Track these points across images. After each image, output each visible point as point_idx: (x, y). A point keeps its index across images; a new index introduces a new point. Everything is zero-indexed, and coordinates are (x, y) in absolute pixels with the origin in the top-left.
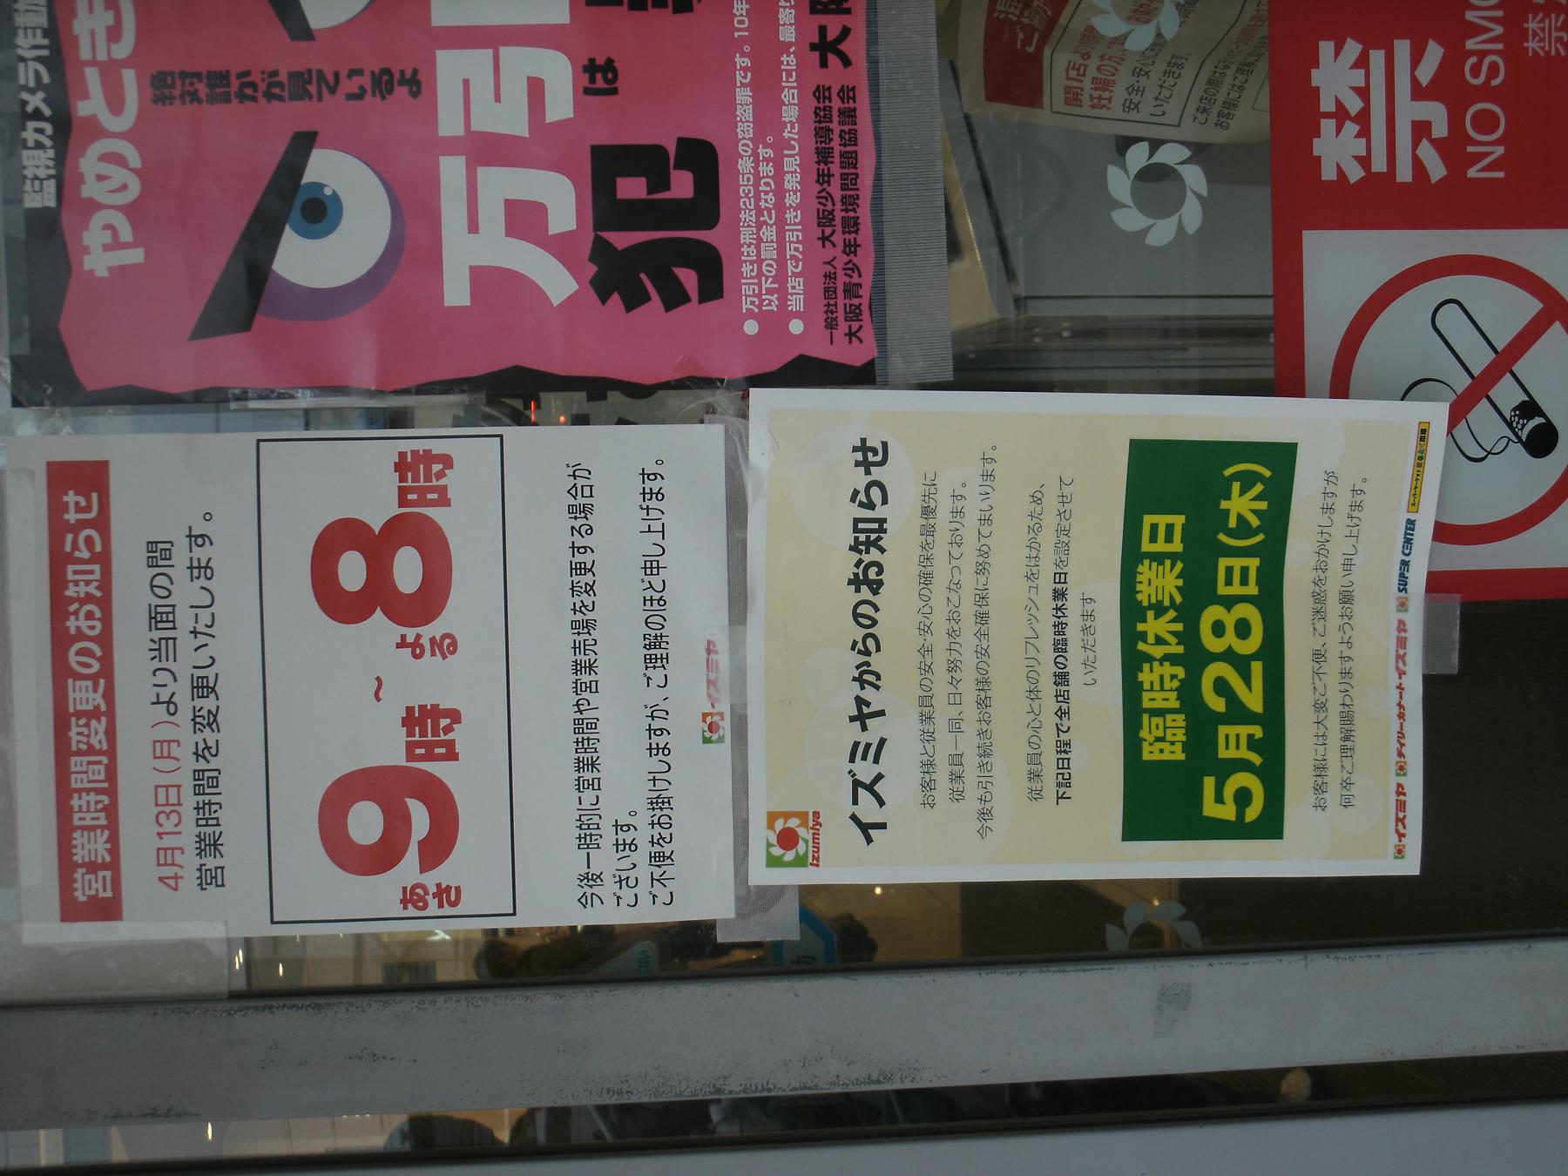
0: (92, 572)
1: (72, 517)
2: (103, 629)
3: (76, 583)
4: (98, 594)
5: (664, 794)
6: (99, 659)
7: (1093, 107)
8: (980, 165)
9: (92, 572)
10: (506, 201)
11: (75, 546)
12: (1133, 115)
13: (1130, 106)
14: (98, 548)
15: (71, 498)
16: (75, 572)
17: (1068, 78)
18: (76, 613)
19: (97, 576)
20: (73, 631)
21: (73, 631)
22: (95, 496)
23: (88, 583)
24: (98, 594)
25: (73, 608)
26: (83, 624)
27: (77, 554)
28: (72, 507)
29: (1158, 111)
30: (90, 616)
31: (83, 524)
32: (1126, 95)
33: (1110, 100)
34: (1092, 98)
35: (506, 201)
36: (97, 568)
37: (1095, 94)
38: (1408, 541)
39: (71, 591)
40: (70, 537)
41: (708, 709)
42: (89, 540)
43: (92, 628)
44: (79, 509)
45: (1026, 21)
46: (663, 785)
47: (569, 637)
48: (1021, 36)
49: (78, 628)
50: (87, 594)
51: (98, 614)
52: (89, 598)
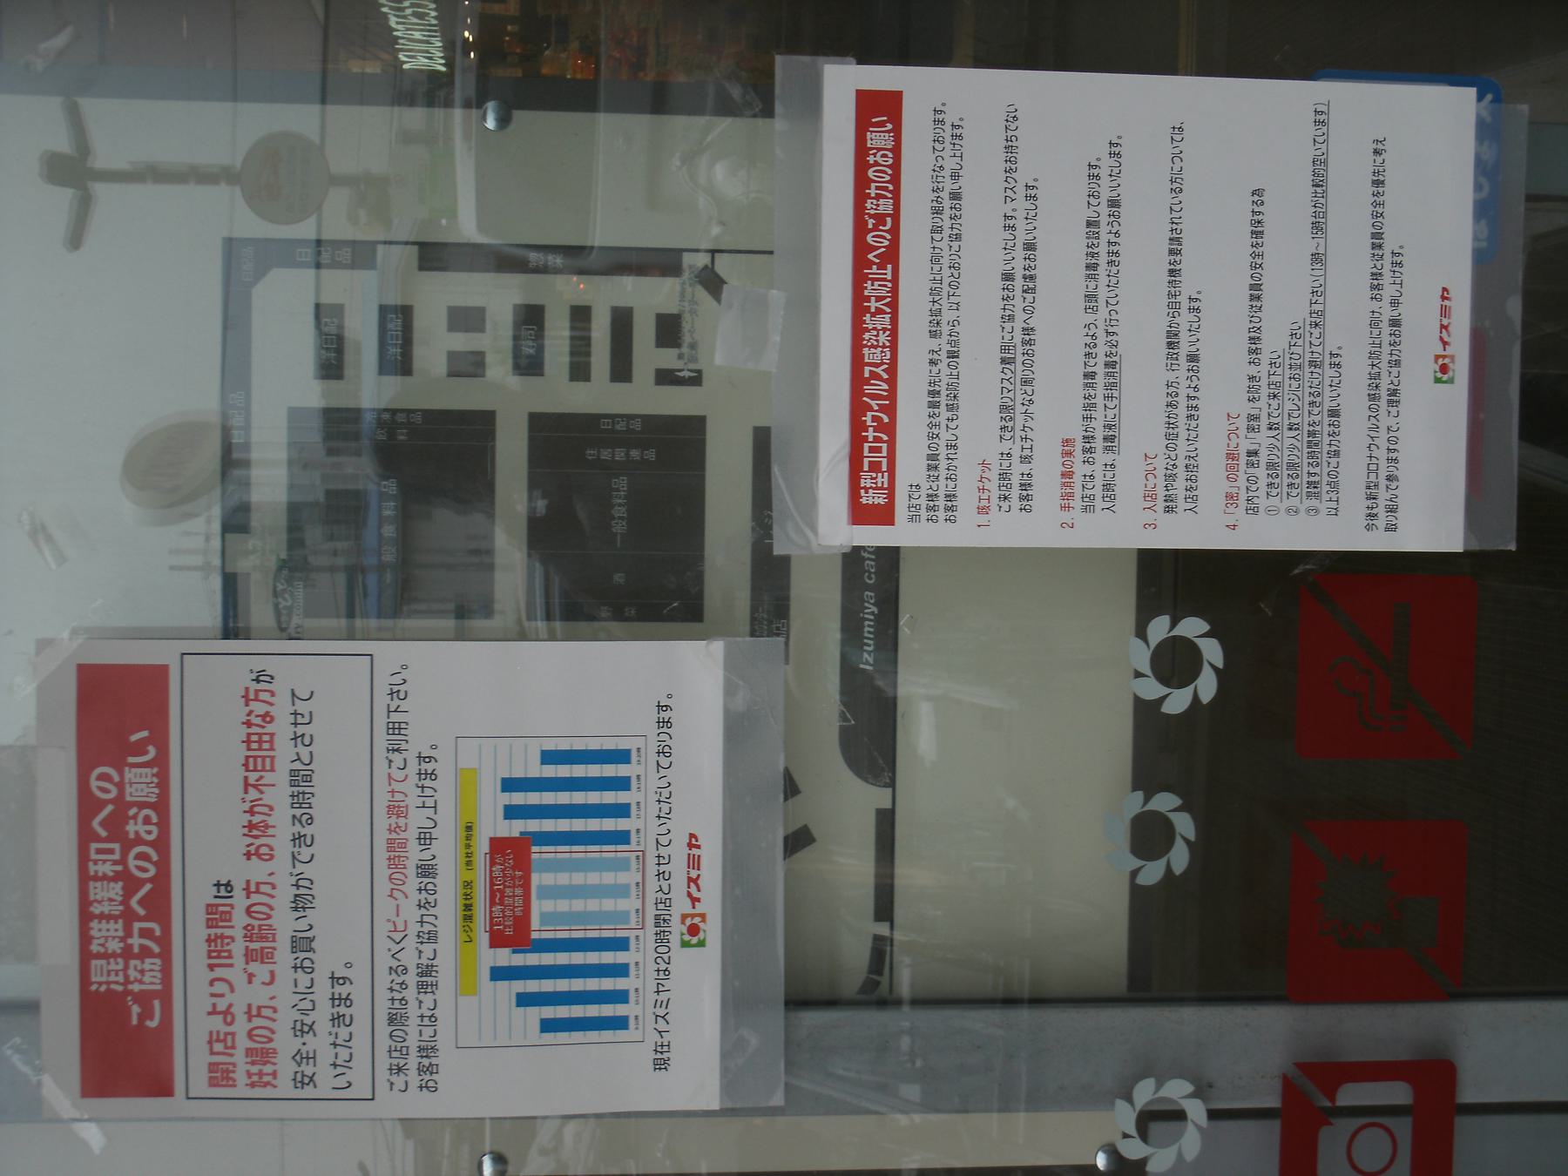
2: (159, 836)
6: (155, 864)
7: (253, 1085)
8: (150, 1120)
10: (859, 93)
12: (308, 1091)
13: (303, 1081)
17: (212, 1053)
18: (135, 817)
20: (132, 836)
21: (132, 836)
25: (132, 812)
29: (341, 1082)
30: (147, 820)
32: (294, 1067)
33: (274, 1074)
34: (249, 1075)
35: (859, 93)
37: (255, 1069)
41: (690, 911)
43: (149, 833)
45: (136, 987)
47: (1249, 241)
48: (136, 1009)
49: (137, 833)
51: (155, 820)
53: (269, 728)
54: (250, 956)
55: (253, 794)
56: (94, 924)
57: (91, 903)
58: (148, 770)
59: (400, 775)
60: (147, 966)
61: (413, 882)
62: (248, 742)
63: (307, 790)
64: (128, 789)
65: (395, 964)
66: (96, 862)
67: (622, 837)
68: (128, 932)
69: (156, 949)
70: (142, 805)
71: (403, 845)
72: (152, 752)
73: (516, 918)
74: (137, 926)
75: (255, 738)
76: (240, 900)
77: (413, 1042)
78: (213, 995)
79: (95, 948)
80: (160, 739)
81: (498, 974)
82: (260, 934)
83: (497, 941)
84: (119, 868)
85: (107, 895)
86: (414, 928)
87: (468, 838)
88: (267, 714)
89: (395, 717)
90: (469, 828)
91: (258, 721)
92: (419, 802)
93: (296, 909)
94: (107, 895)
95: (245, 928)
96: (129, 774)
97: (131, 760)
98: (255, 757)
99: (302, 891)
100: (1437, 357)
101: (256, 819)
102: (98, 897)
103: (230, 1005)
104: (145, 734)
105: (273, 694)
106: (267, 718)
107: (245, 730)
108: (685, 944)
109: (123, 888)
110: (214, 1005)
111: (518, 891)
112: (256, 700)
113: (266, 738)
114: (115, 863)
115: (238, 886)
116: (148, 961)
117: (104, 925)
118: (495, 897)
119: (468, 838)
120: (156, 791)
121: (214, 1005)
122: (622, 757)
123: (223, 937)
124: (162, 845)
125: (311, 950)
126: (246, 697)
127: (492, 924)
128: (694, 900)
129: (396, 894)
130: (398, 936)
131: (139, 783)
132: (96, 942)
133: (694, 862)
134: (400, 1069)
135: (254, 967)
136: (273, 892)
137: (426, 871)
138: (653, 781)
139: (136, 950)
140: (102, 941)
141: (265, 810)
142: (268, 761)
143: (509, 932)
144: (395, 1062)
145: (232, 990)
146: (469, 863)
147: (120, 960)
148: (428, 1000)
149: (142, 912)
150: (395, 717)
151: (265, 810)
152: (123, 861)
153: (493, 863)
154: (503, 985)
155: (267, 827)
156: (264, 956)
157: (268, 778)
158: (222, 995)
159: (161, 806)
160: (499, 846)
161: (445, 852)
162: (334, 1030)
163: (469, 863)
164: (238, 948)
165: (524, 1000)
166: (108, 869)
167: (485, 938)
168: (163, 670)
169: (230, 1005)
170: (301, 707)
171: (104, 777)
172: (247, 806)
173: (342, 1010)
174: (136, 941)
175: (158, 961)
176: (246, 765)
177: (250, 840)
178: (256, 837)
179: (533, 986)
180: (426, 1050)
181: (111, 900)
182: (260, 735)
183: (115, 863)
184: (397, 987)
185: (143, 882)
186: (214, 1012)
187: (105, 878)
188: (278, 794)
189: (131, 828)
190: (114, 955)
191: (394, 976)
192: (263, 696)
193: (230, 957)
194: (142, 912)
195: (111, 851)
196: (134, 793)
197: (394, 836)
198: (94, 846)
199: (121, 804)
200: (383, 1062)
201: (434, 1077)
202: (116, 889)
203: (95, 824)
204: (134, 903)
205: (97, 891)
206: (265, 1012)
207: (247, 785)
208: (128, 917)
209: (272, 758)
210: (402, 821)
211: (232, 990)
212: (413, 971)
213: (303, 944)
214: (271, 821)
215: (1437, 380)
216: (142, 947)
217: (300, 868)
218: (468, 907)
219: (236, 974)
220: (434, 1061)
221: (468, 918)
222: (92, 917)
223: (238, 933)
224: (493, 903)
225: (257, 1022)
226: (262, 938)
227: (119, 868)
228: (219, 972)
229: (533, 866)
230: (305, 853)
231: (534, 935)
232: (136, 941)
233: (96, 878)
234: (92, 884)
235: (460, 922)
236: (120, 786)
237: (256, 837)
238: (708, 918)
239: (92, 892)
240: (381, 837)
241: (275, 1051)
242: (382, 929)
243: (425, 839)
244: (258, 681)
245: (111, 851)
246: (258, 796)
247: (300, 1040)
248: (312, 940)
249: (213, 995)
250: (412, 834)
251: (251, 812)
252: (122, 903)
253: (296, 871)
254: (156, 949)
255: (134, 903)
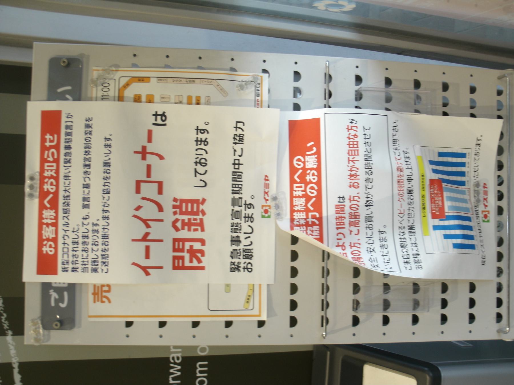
0: (52, 166)
1: (48, 144)
3: (47, 170)
4: (55, 175)
5: (107, 234)
9: (52, 166)
11: (48, 156)
14: (56, 157)
15: (48, 137)
16: (48, 166)
19: (55, 168)
20: (308, 181)
21: (308, 181)
22: (56, 136)
23: (51, 170)
24: (55, 175)
26: (311, 178)
27: (49, 159)
28: (48, 140)
29: (388, 267)
31: (51, 147)
36: (54, 164)
38: (88, 146)
39: (46, 174)
40: (46, 152)
42: (53, 154)
44: (51, 141)
46: (106, 230)
49: (310, 179)
50: (52, 175)
52: (52, 177)
53: (356, 140)
54: (351, 224)
55: (351, 164)
56: (295, 214)
57: (294, 206)
58: (313, 156)
59: (398, 157)
60: (314, 229)
61: (406, 195)
62: (349, 145)
63: (370, 162)
64: (307, 164)
65: (400, 225)
66: (296, 191)
67: (463, 183)
68: (307, 215)
69: (317, 222)
70: (311, 169)
71: (402, 182)
72: (315, 149)
73: (440, 208)
74: (310, 214)
75: (351, 143)
76: (347, 203)
77: (410, 253)
78: (338, 239)
79: (295, 223)
80: (318, 145)
81: (436, 228)
82: (355, 216)
83: (434, 216)
84: (304, 193)
85: (300, 202)
86: (407, 212)
87: (423, 179)
88: (355, 135)
89: (395, 138)
90: (423, 176)
91: (352, 137)
92: (406, 166)
93: (367, 206)
94: (299, 203)
95: (349, 214)
96: (307, 158)
97: (308, 153)
98: (352, 150)
99: (369, 199)
100: (263, 206)
101: (353, 173)
102: (297, 204)
103: (344, 243)
104: (312, 143)
105: (357, 127)
106: (355, 136)
107: (348, 140)
108: (484, 221)
109: (305, 200)
110: (338, 243)
111: (440, 198)
112: (351, 129)
113: (355, 143)
114: (303, 191)
115: (347, 198)
116: (315, 227)
117: (299, 214)
118: (433, 201)
119: (423, 179)
120: (317, 163)
121: (338, 243)
122: (463, 155)
123: (341, 217)
124: (319, 183)
125: (372, 221)
126: (348, 128)
127: (432, 210)
128: (486, 206)
129: (401, 200)
130: (401, 215)
131: (311, 161)
132: (296, 220)
133: (486, 193)
134: (408, 262)
135: (353, 228)
136: (358, 200)
137: (410, 191)
138: (473, 164)
139: (310, 223)
140: (298, 220)
141: (356, 169)
142: (356, 151)
143: (438, 213)
144: (405, 260)
145: (344, 237)
146: (423, 188)
147: (305, 227)
148: (413, 238)
149: (312, 209)
150: (395, 138)
151: (356, 169)
152: (305, 190)
153: (431, 189)
154: (438, 232)
155: (357, 176)
156: (355, 224)
157: (357, 158)
158: (340, 239)
159: (318, 169)
160: (432, 182)
161: (416, 184)
162: (382, 250)
163: (423, 188)
164: (347, 221)
165: (446, 237)
166: (300, 193)
167: (429, 215)
168: (318, 120)
169: (344, 243)
170: (367, 132)
171: (299, 160)
172: (349, 168)
173: (384, 243)
174: (310, 220)
175: (318, 227)
176: (348, 153)
177: (351, 181)
178: (353, 180)
179: (448, 232)
180: (416, 255)
181: (301, 205)
182: (353, 142)
183: (303, 191)
184: (401, 234)
185: (312, 198)
186: (338, 246)
187: (299, 197)
188: (360, 164)
189: (308, 178)
190: (302, 225)
191: (400, 230)
192: (354, 128)
193: (344, 225)
194: (312, 209)
195: (301, 187)
196: (309, 165)
197: (399, 179)
198: (295, 185)
199: (304, 169)
200: (401, 260)
201: (420, 264)
202: (303, 200)
203: (296, 177)
204: (309, 205)
205: (296, 201)
206: (357, 245)
207: (349, 160)
208: (307, 211)
209: (358, 150)
210: (402, 173)
211: (344, 237)
212: (407, 228)
213: (369, 219)
214: (358, 174)
215: (263, 217)
216: (312, 222)
217: (368, 190)
218: (424, 204)
219: (346, 231)
220: (419, 259)
221: (424, 208)
222: (295, 211)
223: (347, 215)
224: (432, 203)
225: (354, 249)
226: (355, 217)
227: (304, 193)
228: (340, 231)
229: (444, 189)
230: (370, 185)
231: (447, 214)
232: (310, 220)
233: (296, 197)
234: (294, 199)
235: (422, 210)
236: (304, 163)
237: (353, 180)
238: (491, 213)
239: (294, 202)
240: (396, 179)
241: (362, 258)
242: (396, 212)
243: (410, 180)
244: (352, 123)
245: (301, 187)
246: (353, 164)
247: (370, 255)
248: (372, 217)
249: (338, 239)
250: (405, 178)
251: (351, 170)
252: (305, 206)
253: (367, 192)
254: (317, 222)
255: (309, 205)
